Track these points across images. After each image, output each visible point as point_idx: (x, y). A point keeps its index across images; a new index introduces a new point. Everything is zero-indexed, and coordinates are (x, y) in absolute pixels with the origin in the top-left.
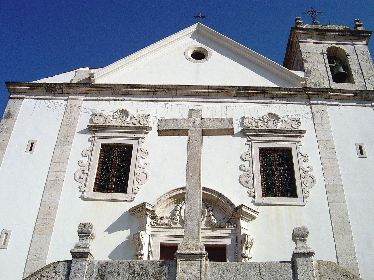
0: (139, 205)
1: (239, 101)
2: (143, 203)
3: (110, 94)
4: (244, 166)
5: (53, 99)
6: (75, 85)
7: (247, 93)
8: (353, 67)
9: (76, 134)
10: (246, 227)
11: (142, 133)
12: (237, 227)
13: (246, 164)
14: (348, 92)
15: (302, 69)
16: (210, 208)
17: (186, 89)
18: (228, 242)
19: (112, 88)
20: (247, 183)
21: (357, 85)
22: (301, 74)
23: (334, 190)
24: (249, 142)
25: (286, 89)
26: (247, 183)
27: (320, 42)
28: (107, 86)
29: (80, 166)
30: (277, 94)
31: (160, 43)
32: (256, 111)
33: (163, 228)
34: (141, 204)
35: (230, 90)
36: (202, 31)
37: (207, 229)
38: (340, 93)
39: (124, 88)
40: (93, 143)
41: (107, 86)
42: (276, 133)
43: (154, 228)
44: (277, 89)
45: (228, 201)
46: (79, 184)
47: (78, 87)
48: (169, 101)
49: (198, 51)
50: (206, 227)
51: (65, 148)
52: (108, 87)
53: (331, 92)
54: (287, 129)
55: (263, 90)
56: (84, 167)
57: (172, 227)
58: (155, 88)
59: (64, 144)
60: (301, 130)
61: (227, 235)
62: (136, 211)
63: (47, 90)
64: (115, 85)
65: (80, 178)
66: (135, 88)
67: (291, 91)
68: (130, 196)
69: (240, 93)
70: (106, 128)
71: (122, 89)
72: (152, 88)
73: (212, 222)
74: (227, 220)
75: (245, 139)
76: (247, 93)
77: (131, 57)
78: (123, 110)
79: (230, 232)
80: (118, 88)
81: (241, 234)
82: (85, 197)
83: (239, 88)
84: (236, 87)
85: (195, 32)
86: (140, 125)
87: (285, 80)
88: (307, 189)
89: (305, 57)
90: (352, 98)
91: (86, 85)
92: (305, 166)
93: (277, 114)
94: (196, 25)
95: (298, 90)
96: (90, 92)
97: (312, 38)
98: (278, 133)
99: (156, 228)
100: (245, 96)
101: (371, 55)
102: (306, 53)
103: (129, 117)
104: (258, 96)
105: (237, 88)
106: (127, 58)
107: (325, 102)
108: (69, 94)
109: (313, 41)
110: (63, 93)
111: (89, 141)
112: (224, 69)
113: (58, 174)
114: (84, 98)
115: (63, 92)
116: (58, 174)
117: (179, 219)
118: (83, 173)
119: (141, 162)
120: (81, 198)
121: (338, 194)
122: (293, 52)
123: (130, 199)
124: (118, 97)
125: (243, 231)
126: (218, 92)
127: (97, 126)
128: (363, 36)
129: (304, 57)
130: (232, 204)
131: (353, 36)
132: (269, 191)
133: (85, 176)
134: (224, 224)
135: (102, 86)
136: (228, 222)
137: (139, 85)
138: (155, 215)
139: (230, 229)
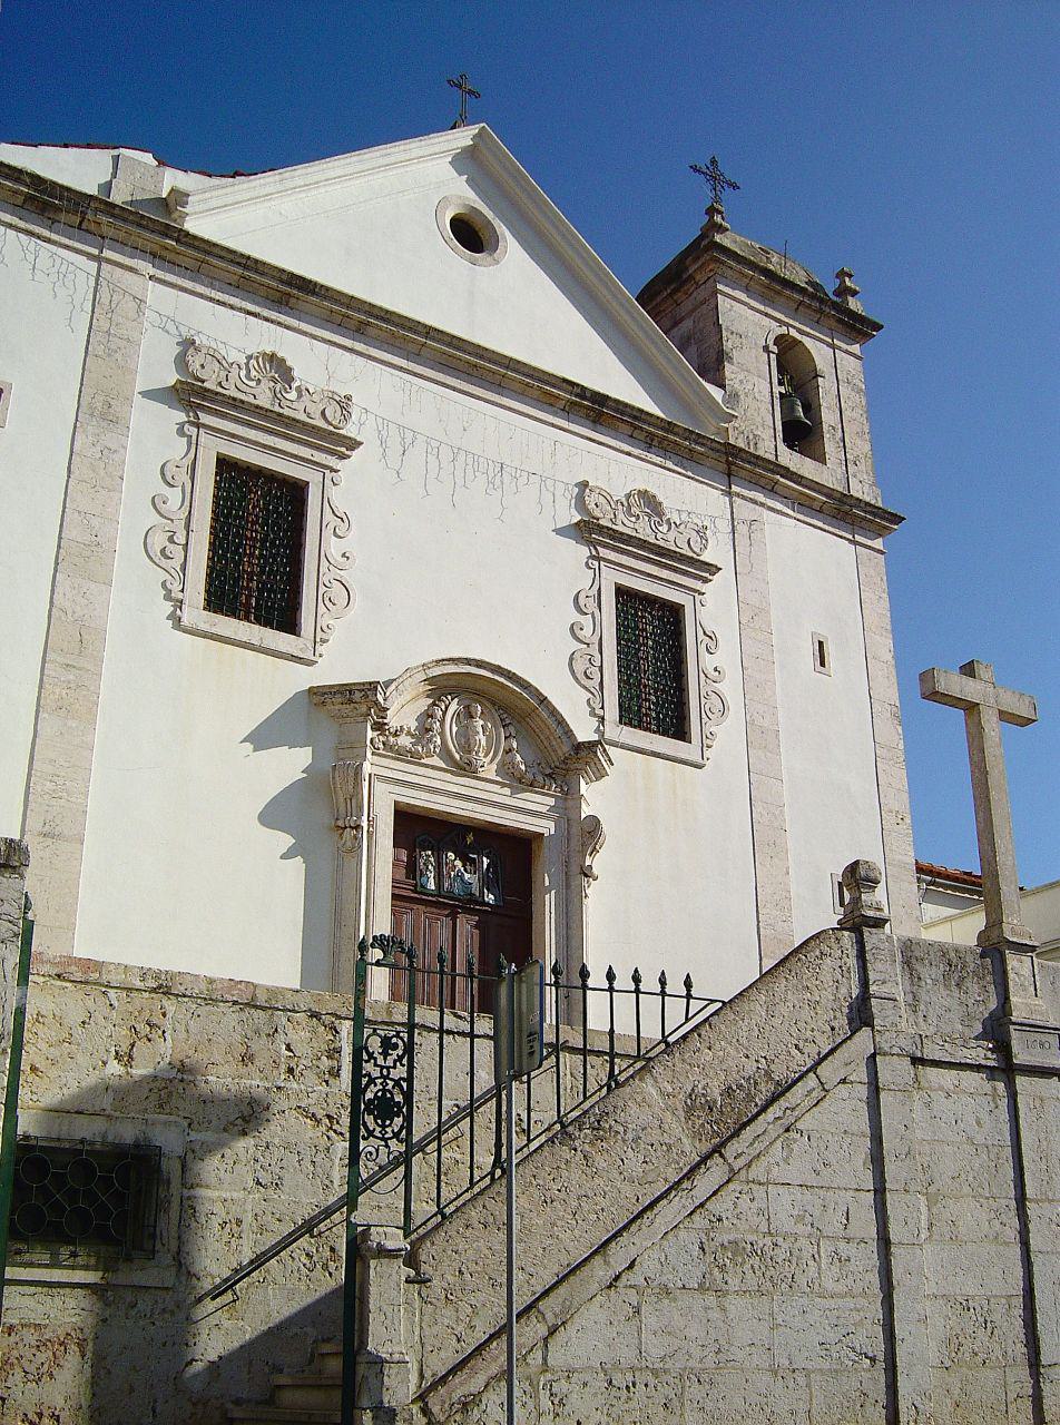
0: (354, 684)
1: (573, 427)
2: (370, 683)
3: (230, 284)
4: (581, 629)
5: (48, 241)
6: (131, 218)
7: (595, 410)
8: (828, 417)
9: (138, 398)
10: (594, 798)
11: (332, 453)
12: (569, 796)
13: (587, 621)
14: (817, 487)
15: (723, 386)
16: (512, 729)
17: (449, 345)
18: (546, 827)
19: (246, 267)
20: (588, 678)
21: (827, 475)
22: (716, 393)
23: (760, 738)
24: (191, 428)
25: (689, 434)
26: (588, 678)
27: (762, 308)
28: (231, 256)
29: (162, 515)
30: (664, 438)
31: (378, 154)
32: (618, 471)
33: (398, 759)
34: (363, 684)
35: (559, 389)
36: (485, 152)
37: (503, 785)
38: (799, 484)
39: (282, 282)
40: (194, 446)
41: (231, 256)
42: (657, 554)
43: (379, 755)
44: (669, 427)
45: (561, 722)
46: (164, 576)
47: (139, 225)
48: (401, 369)
49: (466, 218)
50: (499, 779)
51: (110, 440)
52: (232, 261)
53: (782, 476)
54: (678, 550)
55: (635, 418)
56: (172, 520)
57: (423, 761)
58: (371, 315)
59: (104, 424)
60: (712, 565)
61: (544, 809)
62: (338, 698)
63: (29, 198)
64: (256, 261)
65: (163, 551)
66: (313, 293)
67: (697, 444)
68: (310, 645)
69: (581, 405)
70: (235, 407)
71: (274, 284)
72: (359, 311)
73: (514, 765)
74: (548, 771)
75: (584, 551)
76: (595, 410)
77: (297, 173)
78: (643, 494)
79: (551, 802)
80: (262, 274)
81: (583, 816)
82: (185, 621)
83: (582, 391)
84: (578, 385)
85: (465, 150)
86: (325, 426)
87: (687, 407)
88: (710, 728)
89: (730, 344)
90: (816, 505)
91: (141, 222)
92: (709, 662)
93: (660, 498)
94: (474, 130)
95: (714, 445)
96: (170, 256)
97: (747, 290)
98: (661, 555)
99: (385, 756)
100: (588, 417)
101: (868, 393)
102: (732, 333)
103: (294, 385)
104: (616, 430)
105: (579, 391)
106: (287, 173)
107: (760, 497)
108: (101, 239)
109: (747, 300)
110: (82, 229)
111: (181, 432)
112: (522, 306)
113: (95, 522)
114: (152, 271)
115: (81, 223)
116: (95, 522)
117: (439, 742)
118: (171, 540)
119: (334, 547)
120: (171, 622)
121: (769, 754)
122: (676, 302)
123: (309, 655)
124: (258, 304)
125: (586, 811)
126: (527, 384)
127: (334, 434)
128: (859, 332)
129: (727, 346)
130: (569, 733)
131: (840, 321)
132: (221, 597)
133: (178, 552)
134: (540, 778)
135: (215, 250)
136: (550, 776)
137: (328, 289)
138: (385, 721)
139: (552, 796)
